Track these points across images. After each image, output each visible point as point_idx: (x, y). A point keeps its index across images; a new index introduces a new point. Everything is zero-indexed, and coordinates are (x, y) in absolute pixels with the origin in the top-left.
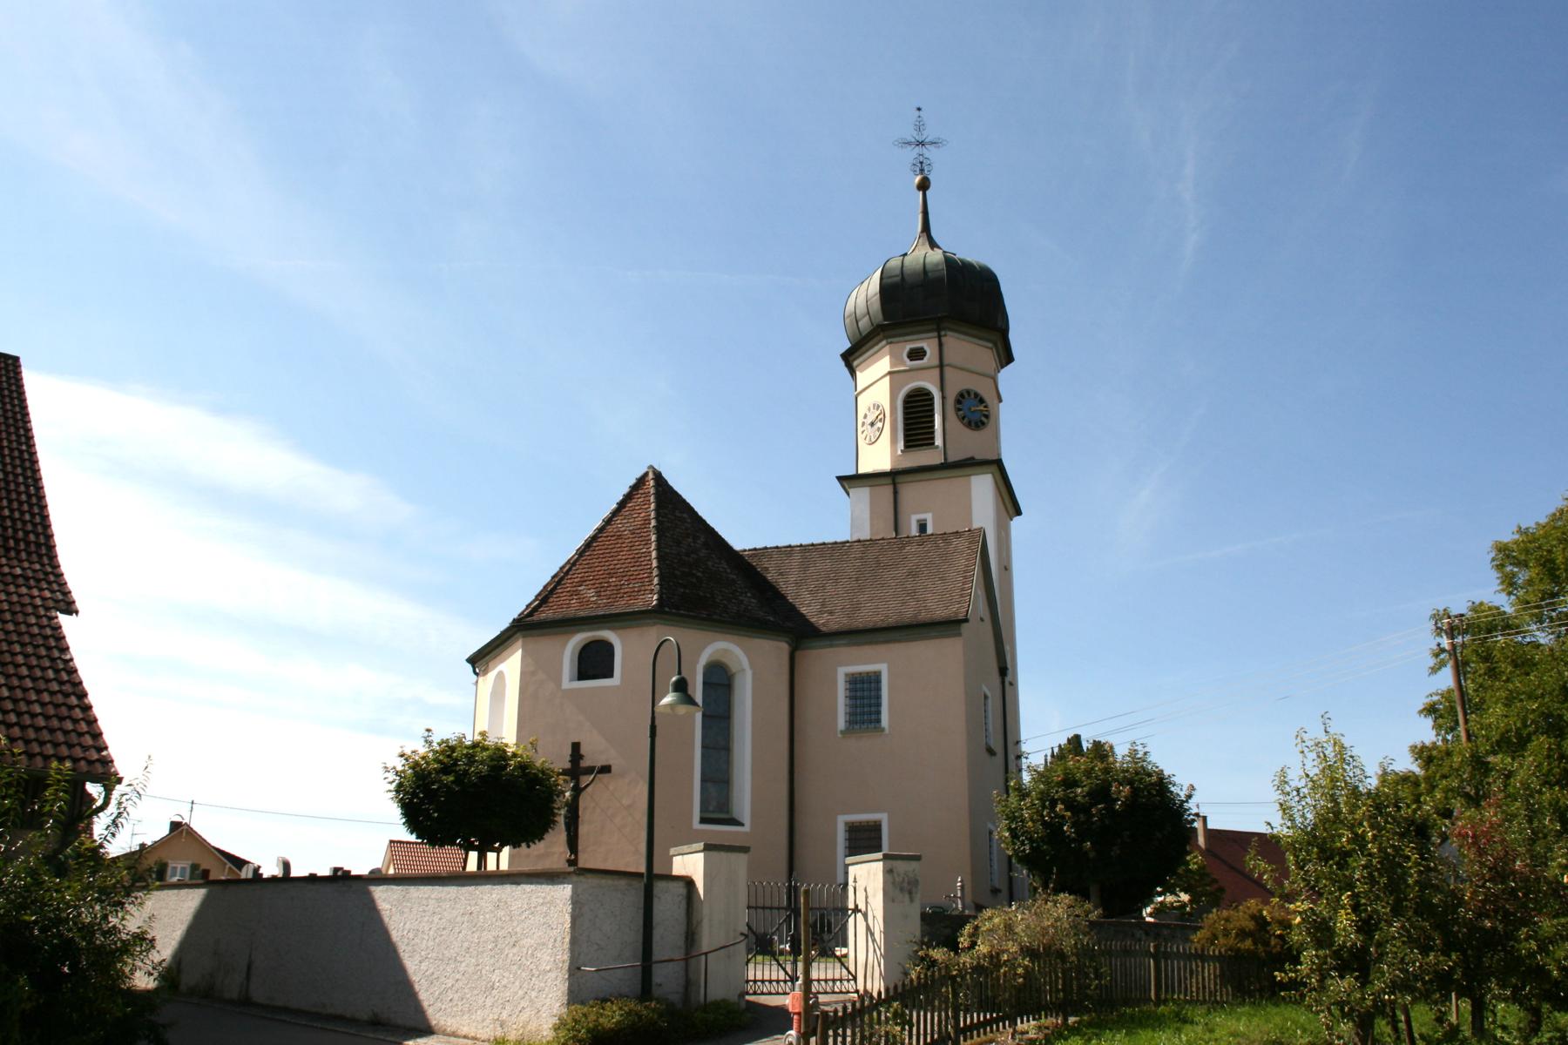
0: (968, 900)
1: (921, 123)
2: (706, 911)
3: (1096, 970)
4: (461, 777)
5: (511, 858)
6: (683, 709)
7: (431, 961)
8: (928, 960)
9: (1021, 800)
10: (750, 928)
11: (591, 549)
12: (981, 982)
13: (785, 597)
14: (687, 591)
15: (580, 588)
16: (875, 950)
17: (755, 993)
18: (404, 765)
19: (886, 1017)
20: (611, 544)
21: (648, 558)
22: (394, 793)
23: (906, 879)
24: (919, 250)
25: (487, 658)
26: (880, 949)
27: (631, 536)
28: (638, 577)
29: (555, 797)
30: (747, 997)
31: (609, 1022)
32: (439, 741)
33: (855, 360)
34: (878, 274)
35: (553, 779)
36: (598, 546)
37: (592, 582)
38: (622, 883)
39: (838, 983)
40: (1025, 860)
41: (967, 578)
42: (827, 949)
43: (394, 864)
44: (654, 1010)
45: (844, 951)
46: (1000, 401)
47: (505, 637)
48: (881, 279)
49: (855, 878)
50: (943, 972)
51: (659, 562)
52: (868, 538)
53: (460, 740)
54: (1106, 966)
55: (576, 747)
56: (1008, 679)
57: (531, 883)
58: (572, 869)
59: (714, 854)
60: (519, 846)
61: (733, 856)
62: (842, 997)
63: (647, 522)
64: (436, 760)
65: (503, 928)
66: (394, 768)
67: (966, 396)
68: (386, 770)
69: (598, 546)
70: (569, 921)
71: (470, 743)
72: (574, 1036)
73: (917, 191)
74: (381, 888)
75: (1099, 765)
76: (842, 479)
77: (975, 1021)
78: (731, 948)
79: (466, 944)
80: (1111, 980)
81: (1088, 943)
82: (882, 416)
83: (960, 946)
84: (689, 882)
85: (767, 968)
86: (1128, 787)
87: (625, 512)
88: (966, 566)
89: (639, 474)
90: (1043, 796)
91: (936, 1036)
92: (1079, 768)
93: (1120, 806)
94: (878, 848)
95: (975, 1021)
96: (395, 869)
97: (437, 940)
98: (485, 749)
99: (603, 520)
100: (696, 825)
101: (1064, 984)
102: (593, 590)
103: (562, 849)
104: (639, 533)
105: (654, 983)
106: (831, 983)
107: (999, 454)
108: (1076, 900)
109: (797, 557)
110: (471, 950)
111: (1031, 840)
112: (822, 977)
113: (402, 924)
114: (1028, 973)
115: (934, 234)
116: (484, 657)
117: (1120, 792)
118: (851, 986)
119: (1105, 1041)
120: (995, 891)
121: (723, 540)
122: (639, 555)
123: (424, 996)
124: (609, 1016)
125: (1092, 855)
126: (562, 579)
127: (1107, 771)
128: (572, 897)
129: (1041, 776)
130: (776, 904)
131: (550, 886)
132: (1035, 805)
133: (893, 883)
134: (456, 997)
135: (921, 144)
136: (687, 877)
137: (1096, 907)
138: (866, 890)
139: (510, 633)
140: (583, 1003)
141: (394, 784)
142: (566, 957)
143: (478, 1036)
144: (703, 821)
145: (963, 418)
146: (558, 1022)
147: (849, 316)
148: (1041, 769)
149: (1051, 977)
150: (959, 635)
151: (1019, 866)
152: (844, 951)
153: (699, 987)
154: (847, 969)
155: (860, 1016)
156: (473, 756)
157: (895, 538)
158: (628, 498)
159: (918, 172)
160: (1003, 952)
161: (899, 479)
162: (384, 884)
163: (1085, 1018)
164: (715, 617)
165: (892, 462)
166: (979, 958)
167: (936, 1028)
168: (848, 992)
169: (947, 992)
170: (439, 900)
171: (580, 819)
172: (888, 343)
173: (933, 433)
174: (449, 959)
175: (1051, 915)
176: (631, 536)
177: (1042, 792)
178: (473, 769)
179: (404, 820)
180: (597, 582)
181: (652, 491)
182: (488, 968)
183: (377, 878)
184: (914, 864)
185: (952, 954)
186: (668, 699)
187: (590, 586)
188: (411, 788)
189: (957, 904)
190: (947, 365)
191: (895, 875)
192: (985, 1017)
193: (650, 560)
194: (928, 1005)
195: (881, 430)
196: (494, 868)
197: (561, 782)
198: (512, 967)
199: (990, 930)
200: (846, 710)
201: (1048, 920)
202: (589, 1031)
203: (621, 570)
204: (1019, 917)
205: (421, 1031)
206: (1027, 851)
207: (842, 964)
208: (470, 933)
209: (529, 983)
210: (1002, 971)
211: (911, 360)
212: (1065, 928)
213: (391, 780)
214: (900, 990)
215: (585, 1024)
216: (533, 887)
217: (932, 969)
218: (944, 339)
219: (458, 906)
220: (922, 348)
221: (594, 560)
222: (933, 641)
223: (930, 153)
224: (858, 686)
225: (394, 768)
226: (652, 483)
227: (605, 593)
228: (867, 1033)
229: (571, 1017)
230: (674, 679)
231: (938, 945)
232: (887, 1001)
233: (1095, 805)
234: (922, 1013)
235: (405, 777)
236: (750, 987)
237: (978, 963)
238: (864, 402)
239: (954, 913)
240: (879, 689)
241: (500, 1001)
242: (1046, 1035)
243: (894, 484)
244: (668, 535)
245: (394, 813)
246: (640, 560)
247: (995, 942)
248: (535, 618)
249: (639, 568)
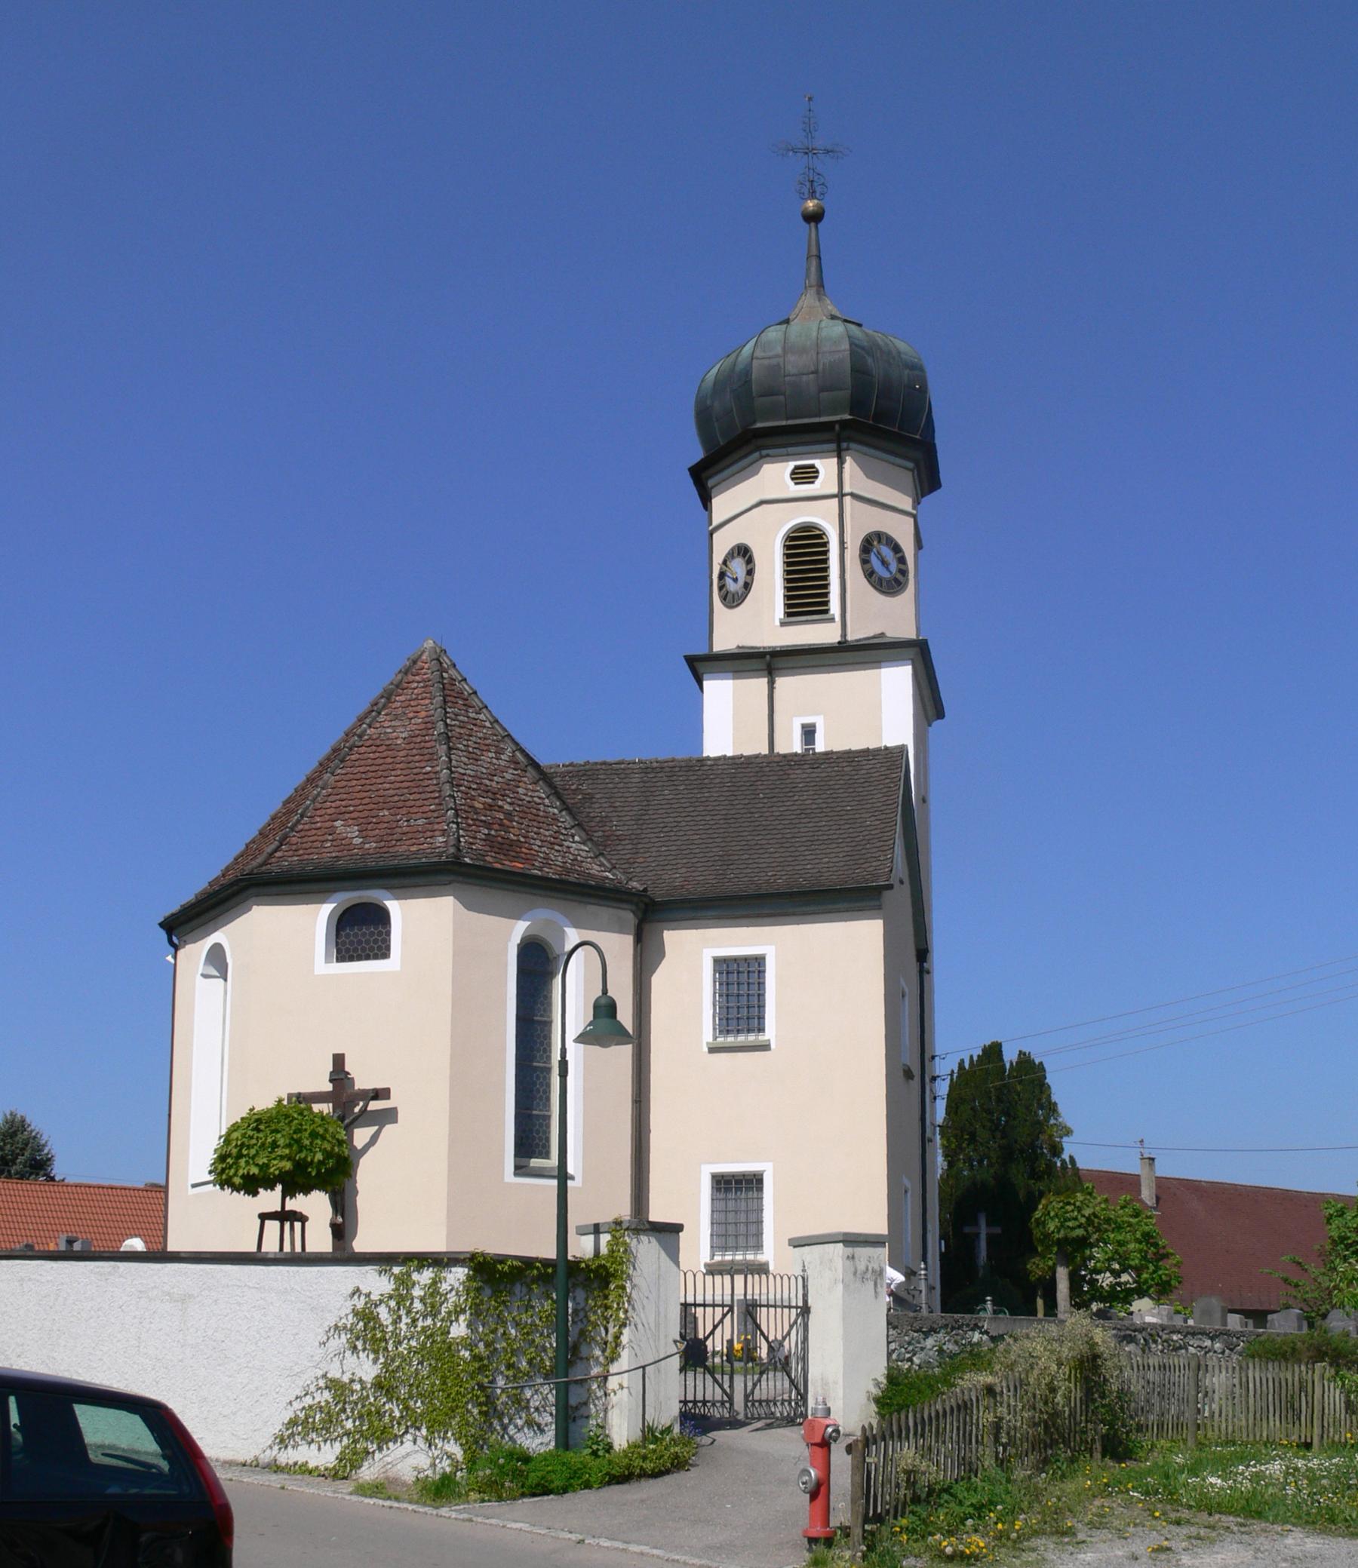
27: (407, 747)
33: (711, 477)
55: (339, 1060)
150: (879, 908)
161: (780, 662)
176: (407, 747)
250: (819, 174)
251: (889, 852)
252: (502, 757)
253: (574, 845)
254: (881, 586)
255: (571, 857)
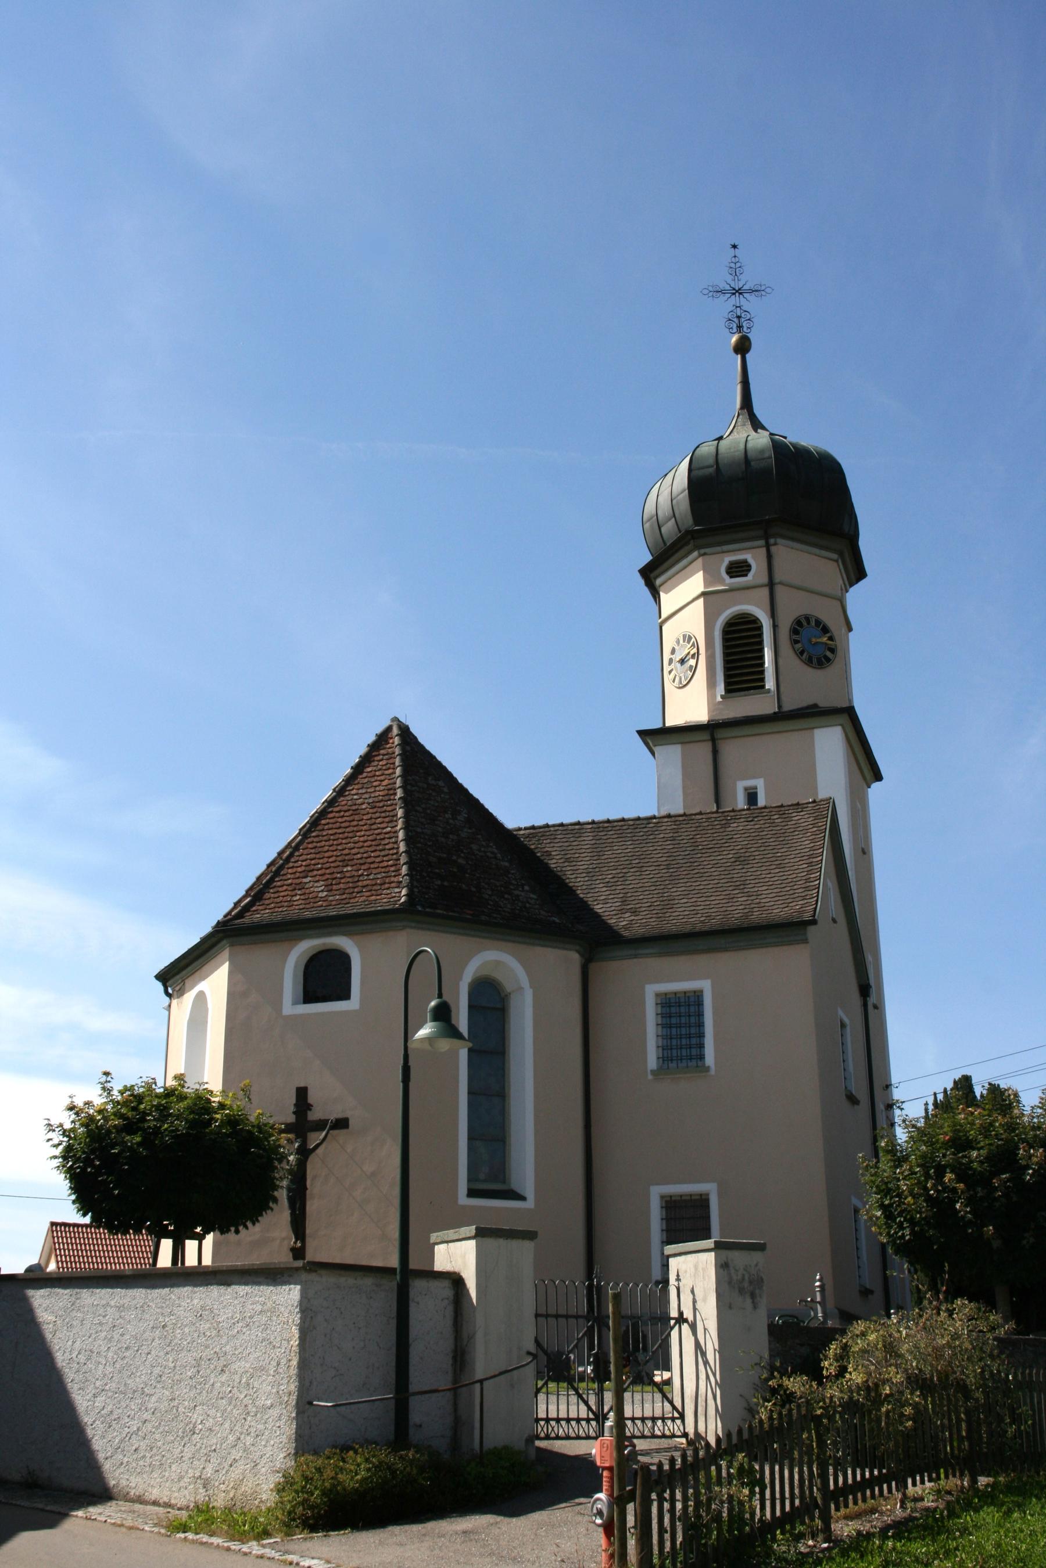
0: (830, 1304)
1: (738, 265)
2: (480, 1320)
3: (1012, 1411)
4: (151, 1137)
5: (216, 1246)
6: (445, 1045)
7: (110, 1394)
8: (782, 1392)
9: (896, 1167)
10: (537, 1342)
11: (320, 827)
12: (856, 1425)
13: (575, 891)
14: (446, 883)
15: (305, 880)
16: (708, 1377)
17: (547, 1437)
18: (73, 1122)
19: (728, 1473)
20: (345, 821)
21: (393, 840)
22: (61, 1160)
23: (746, 1278)
24: (738, 433)
25: (184, 973)
26: (714, 1375)
28: (381, 865)
29: (276, 1163)
30: (538, 1443)
31: (352, 1478)
32: (121, 1088)
34: (685, 464)
35: (274, 1138)
36: (328, 824)
37: (320, 872)
38: (368, 1281)
39: (659, 1423)
40: (904, 1249)
41: (813, 867)
42: (644, 1374)
43: (57, 1256)
44: (412, 1462)
45: (666, 1375)
46: (850, 629)
47: (206, 945)
48: (690, 470)
49: (678, 1275)
50: (803, 1411)
51: (407, 845)
52: (681, 812)
53: (149, 1086)
54: (1025, 1404)
55: (302, 1093)
56: (872, 1000)
57: (246, 1284)
58: (299, 1263)
59: (490, 1242)
60: (228, 1231)
61: (515, 1244)
62: (664, 1443)
63: (391, 792)
64: (117, 1114)
65: (207, 1347)
66: (61, 1125)
67: (805, 624)
68: (50, 1127)
69: (328, 824)
70: (297, 1336)
71: (162, 1090)
72: (305, 1500)
73: (734, 354)
74: (42, 1292)
75: (1000, 1120)
76: (644, 734)
77: (850, 1481)
78: (515, 1372)
79: (157, 1371)
80: (1034, 1424)
81: (999, 1372)
82: (695, 650)
83: (824, 1372)
84: (456, 1281)
85: (563, 1400)
86: (1041, 1150)
87: (362, 779)
88: (812, 849)
89: (379, 729)
90: (926, 1162)
91: (797, 1502)
92: (973, 1124)
93: (1032, 1176)
94: (704, 1233)
95: (850, 1481)
96: (57, 1262)
97: (118, 1366)
98: (182, 1097)
99: (334, 790)
100: (463, 1200)
101: (968, 1431)
102: (322, 883)
103: (284, 1234)
104: (381, 807)
105: (411, 1423)
106: (649, 1423)
107: (850, 701)
108: (979, 1309)
109: (588, 838)
110: (163, 1378)
111: (912, 1222)
112: (638, 1414)
113: (70, 1343)
114: (919, 1414)
115: (757, 410)
116: (178, 973)
117: (1030, 1157)
118: (676, 1427)
119: (1032, 1515)
120: (866, 1292)
121: (491, 815)
122: (382, 836)
123: (100, 1444)
124: (351, 1471)
125: (996, 1244)
126: (281, 867)
127: (1011, 1127)
128: (301, 1303)
129: (921, 1134)
130: (573, 1311)
131: (272, 1288)
132: (916, 1173)
133: (730, 1283)
134: (143, 1445)
135: (738, 292)
136: (455, 1273)
137: (1006, 1320)
138: (692, 1292)
139: (214, 940)
140: (316, 1453)
141: (61, 1148)
142: (293, 1387)
143: (173, 1502)
144: (472, 1193)
145: (802, 653)
146: (282, 1480)
147: (649, 520)
148: (921, 1124)
149: (950, 1420)
150: (805, 941)
151: (897, 1258)
152: (666, 1375)
153: (473, 1428)
154: (671, 1403)
155: (693, 1474)
156: (166, 1108)
157: (717, 812)
158: (366, 760)
159: (735, 330)
160: (885, 1382)
161: (720, 734)
162: (46, 1287)
163: (1001, 1479)
164: (483, 918)
165: (710, 711)
166: (851, 1391)
167: (797, 1491)
168: (673, 1436)
169: (810, 1438)
170: (120, 1308)
171: (308, 1192)
172: (700, 555)
173: (762, 672)
174: (135, 1391)
175: (945, 1329)
177: (924, 1156)
178: (166, 1126)
179: (73, 1197)
180: (328, 871)
181: (397, 751)
182: (186, 1403)
183: (35, 1277)
184: (757, 1256)
185: (814, 1384)
186: (424, 1032)
187: (317, 878)
188: (84, 1152)
189: (816, 1313)
190: (781, 583)
191: (732, 1271)
192: (863, 1475)
193: (396, 842)
194: (783, 1457)
195: (694, 670)
196: (195, 1263)
197: (284, 1142)
198: (220, 1401)
199: (864, 1351)
200: (657, 1042)
201: (943, 1336)
202: (324, 1493)
203: (359, 856)
204: (904, 1333)
205: (93, 1496)
206: (907, 1238)
207: (664, 1396)
208: (162, 1354)
209: (242, 1425)
210: (884, 1409)
211: (731, 577)
212: (966, 1349)
213: (56, 1141)
214: (746, 1436)
215: (320, 1483)
216: (247, 1289)
217: (787, 1406)
218: (773, 549)
219: (147, 1316)
220: (745, 561)
221: (323, 843)
222: (770, 949)
223: (750, 303)
224: (673, 1010)
225: (61, 1125)
226: (397, 740)
227: (338, 887)
228: (704, 1498)
229: (299, 1474)
230: (433, 1004)
231: (794, 1372)
232: (727, 1447)
233: (996, 1174)
234: (777, 1468)
235: (75, 1138)
236: (541, 1429)
237: (851, 1398)
238: (671, 633)
239: (812, 1325)
240: (700, 1014)
241: (203, 1451)
242: (948, 1503)
243: (713, 740)
244: (418, 808)
245: (61, 1184)
246: (383, 842)
247: (872, 1368)
248: (247, 920)
249: (383, 853)
250: (745, 311)
251: (814, 891)
252: (459, 818)
253: (523, 894)
254: (812, 663)
255: (520, 904)
